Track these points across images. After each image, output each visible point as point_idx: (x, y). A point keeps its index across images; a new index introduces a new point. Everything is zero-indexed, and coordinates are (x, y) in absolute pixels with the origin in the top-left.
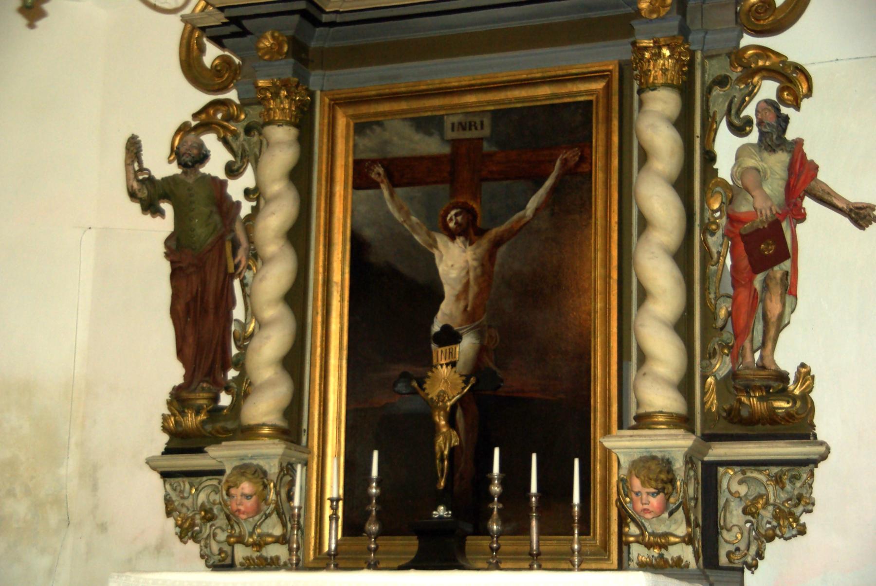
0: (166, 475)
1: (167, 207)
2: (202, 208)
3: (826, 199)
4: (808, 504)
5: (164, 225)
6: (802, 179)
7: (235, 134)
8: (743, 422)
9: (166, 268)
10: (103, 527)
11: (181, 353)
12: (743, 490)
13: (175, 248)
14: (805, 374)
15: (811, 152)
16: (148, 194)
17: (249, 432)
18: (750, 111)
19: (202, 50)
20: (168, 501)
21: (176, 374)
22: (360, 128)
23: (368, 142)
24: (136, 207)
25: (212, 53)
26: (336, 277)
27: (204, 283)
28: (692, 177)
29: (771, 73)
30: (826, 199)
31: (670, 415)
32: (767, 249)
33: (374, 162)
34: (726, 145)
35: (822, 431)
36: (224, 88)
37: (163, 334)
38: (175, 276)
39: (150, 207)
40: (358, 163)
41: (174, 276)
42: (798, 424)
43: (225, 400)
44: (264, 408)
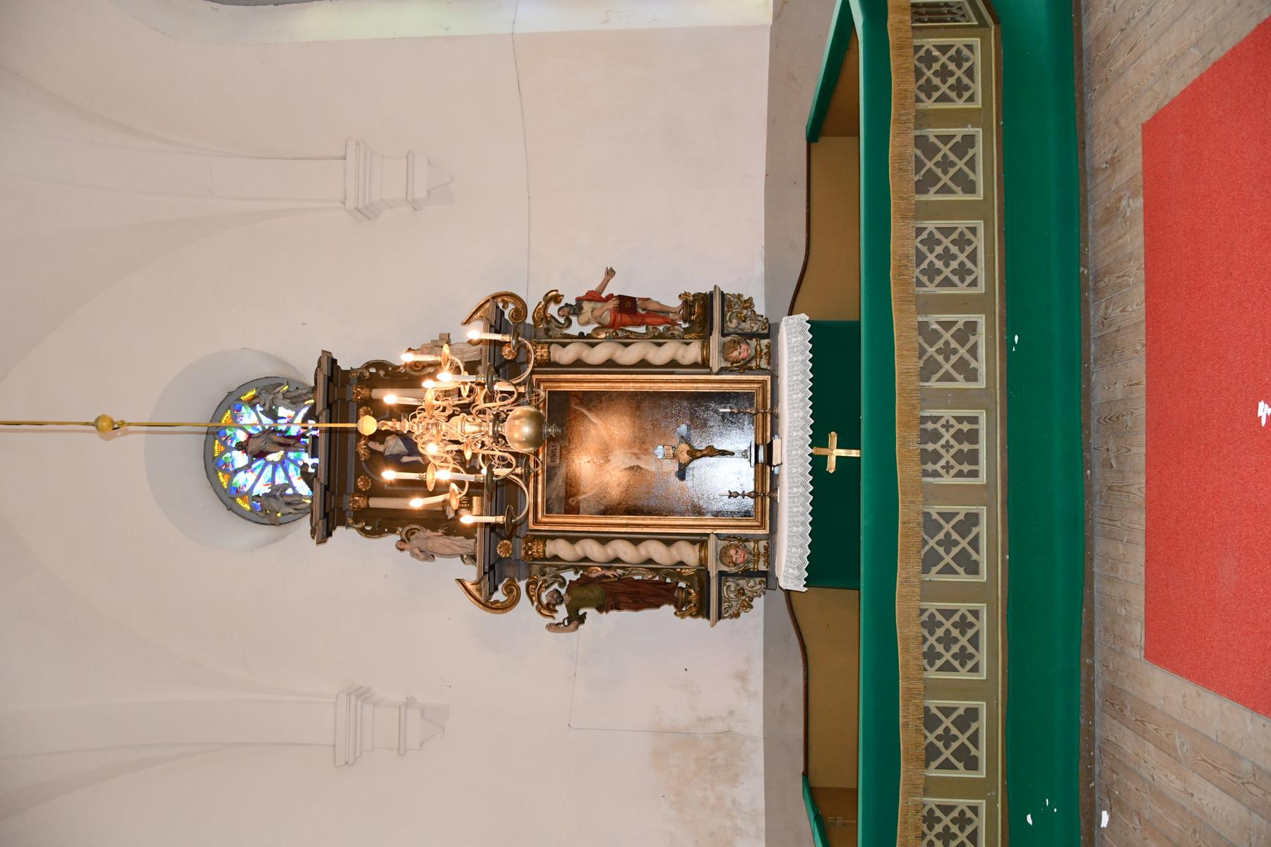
0: (720, 617)
1: (581, 612)
2: (585, 592)
3: (604, 286)
4: (740, 296)
5: (591, 613)
6: (593, 297)
7: (545, 581)
8: (705, 320)
9: (613, 613)
10: (731, 713)
11: (658, 606)
12: (735, 321)
13: (601, 609)
14: (683, 296)
15: (582, 294)
16: (576, 619)
17: (703, 561)
18: (562, 320)
19: (497, 601)
20: (731, 617)
21: (669, 609)
22: (549, 510)
23: (556, 508)
24: (581, 627)
25: (499, 596)
26: (624, 522)
27: (624, 593)
28: (589, 340)
29: (546, 307)
30: (604, 286)
31: (702, 348)
32: (627, 306)
33: (567, 503)
34: (575, 329)
35: (706, 289)
36: (518, 589)
37: (647, 616)
38: (618, 607)
39: (582, 619)
40: (566, 513)
41: (618, 609)
42: (705, 300)
43: (682, 584)
44: (689, 554)
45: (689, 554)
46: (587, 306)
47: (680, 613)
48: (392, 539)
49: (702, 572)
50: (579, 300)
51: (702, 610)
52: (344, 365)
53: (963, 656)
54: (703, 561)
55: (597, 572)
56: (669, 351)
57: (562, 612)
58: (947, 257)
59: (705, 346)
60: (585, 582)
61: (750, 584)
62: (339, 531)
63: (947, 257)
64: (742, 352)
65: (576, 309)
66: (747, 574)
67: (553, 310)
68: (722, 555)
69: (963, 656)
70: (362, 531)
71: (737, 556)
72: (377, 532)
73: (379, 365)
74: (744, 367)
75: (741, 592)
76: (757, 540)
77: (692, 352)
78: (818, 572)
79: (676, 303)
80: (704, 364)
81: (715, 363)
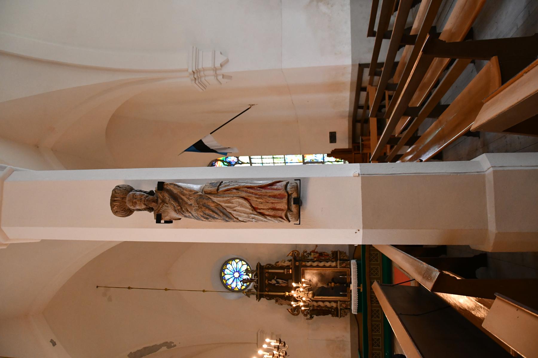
5: (315, 316)
6: (313, 251)
16: (311, 317)
17: (337, 306)
21: (330, 315)
25: (296, 312)
34: (310, 258)
35: (336, 250)
39: (313, 317)
44: (334, 305)
45: (334, 305)
46: (312, 254)
47: (333, 316)
48: (273, 301)
49: (337, 308)
50: (311, 252)
51: (337, 316)
52: (262, 265)
53: (376, 274)
54: (337, 306)
55: (316, 308)
56: (328, 264)
57: (309, 316)
58: (374, 271)
59: (337, 263)
60: (313, 310)
61: (346, 311)
62: (262, 299)
63: (374, 271)
64: (344, 265)
65: (310, 254)
66: (346, 309)
67: (305, 254)
68: (341, 305)
69: (376, 274)
70: (267, 299)
71: (344, 305)
72: (270, 299)
73: (270, 265)
74: (345, 267)
75: (345, 312)
76: (348, 301)
77: (334, 264)
78: (359, 310)
79: (330, 253)
80: (336, 267)
81: (338, 266)
